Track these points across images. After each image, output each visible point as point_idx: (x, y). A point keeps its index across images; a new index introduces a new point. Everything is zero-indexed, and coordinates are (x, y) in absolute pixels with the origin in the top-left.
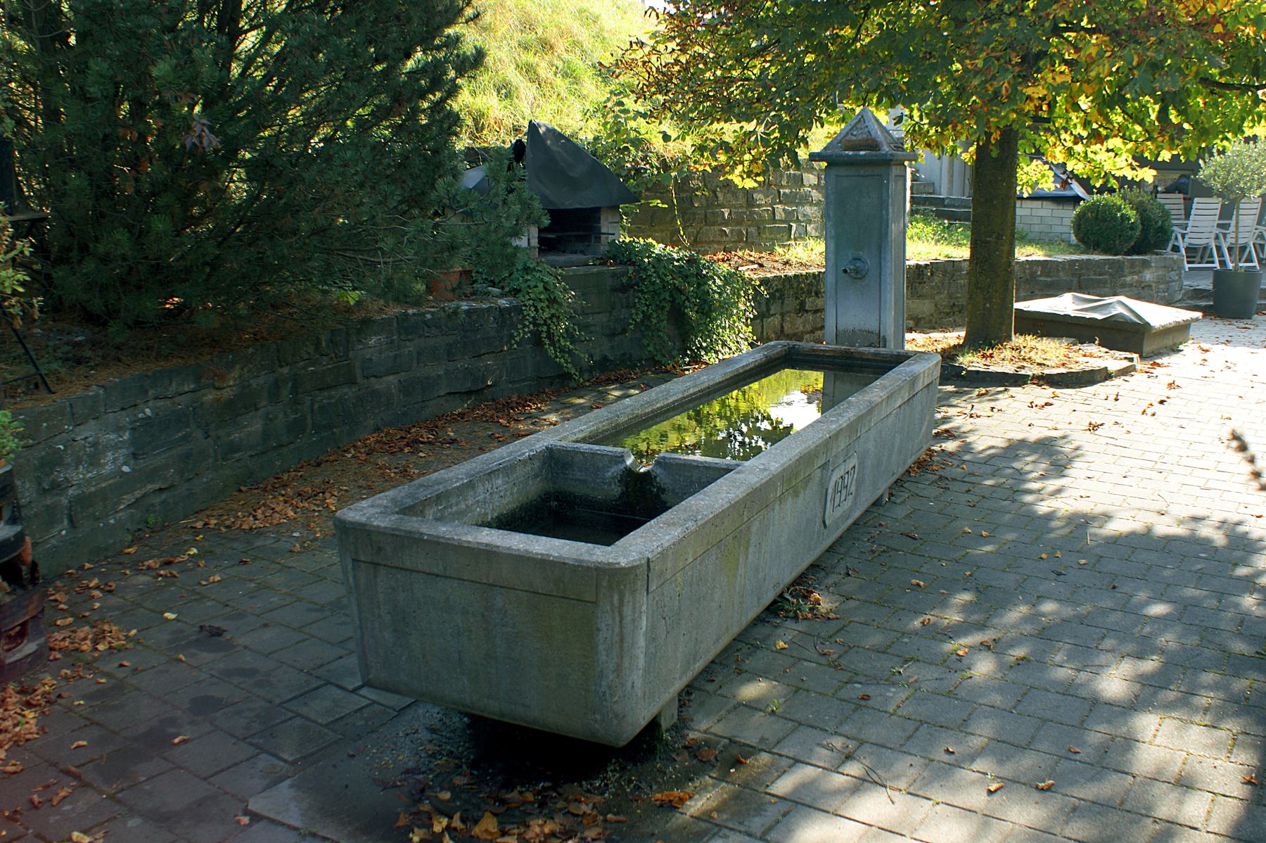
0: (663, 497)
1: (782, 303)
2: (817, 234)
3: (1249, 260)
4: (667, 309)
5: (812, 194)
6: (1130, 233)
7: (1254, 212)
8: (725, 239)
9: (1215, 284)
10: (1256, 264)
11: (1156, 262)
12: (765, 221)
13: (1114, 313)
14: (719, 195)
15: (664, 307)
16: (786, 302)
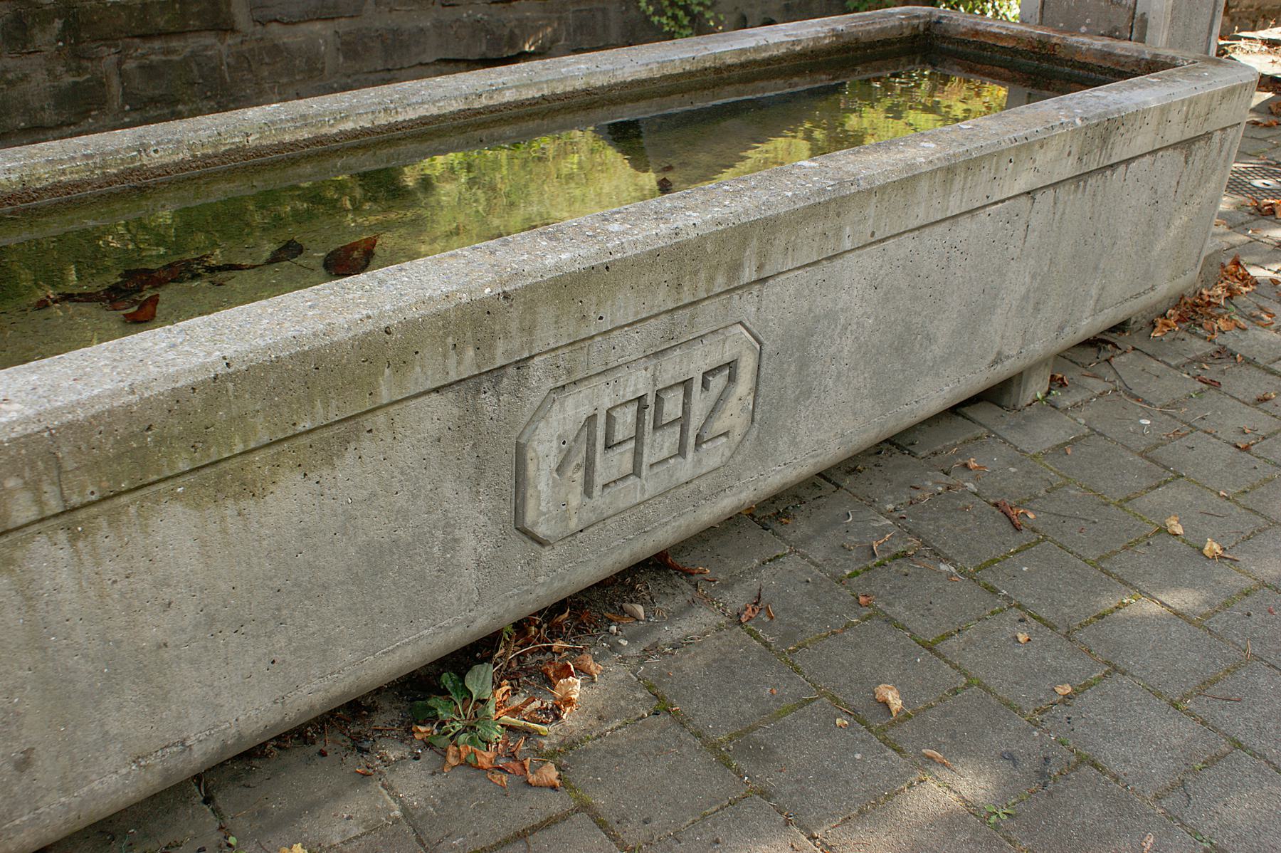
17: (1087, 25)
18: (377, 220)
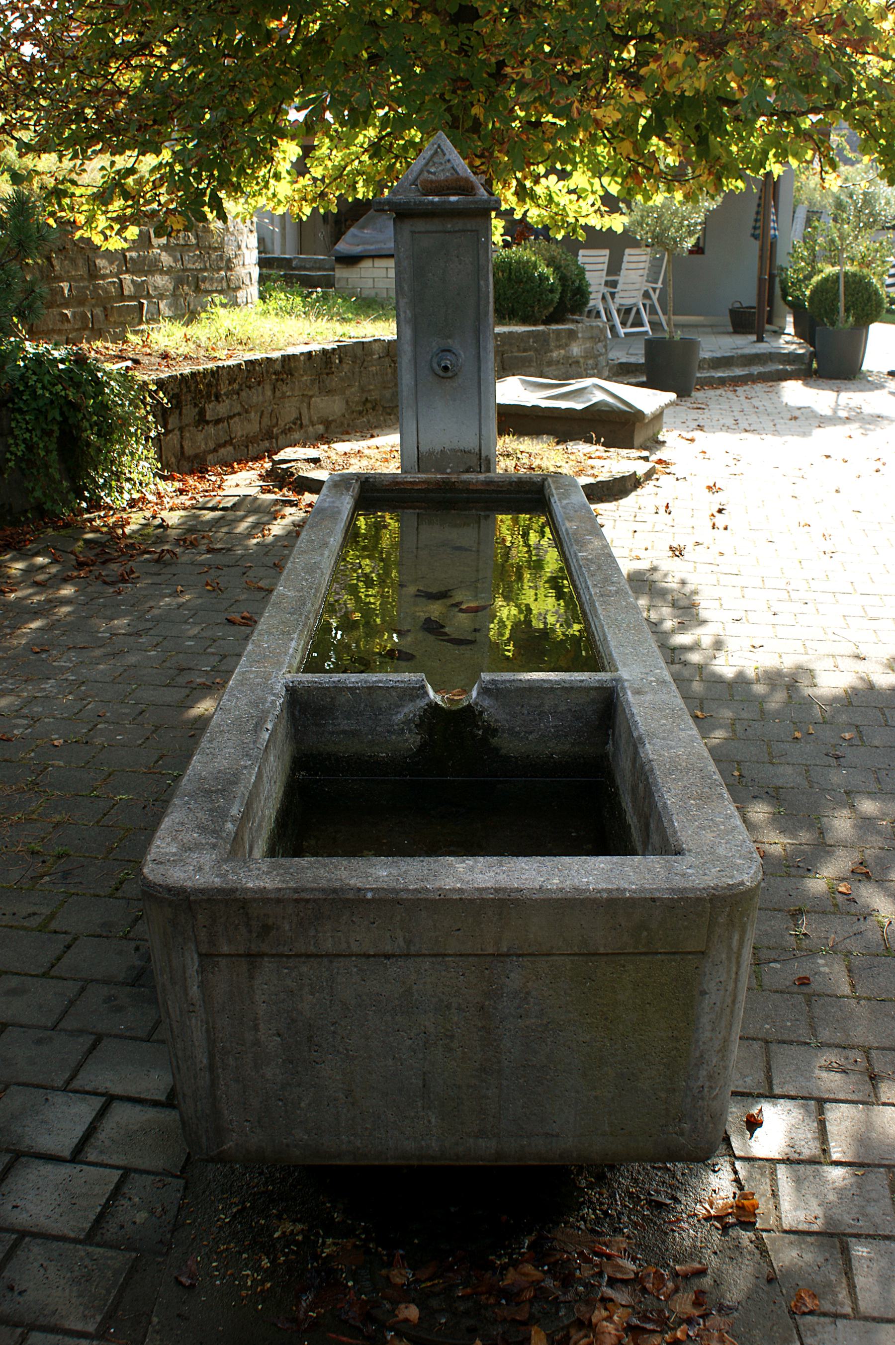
0: (495, 741)
1: (180, 414)
2: (171, 314)
3: (638, 323)
4: (57, 434)
5: (162, 258)
6: (550, 296)
7: (642, 265)
8: (66, 326)
9: (648, 355)
10: (647, 328)
11: (583, 332)
12: (110, 299)
13: (594, 400)
14: (55, 262)
15: (52, 431)
16: (184, 411)
17: (451, 468)
18: (847, 310)
